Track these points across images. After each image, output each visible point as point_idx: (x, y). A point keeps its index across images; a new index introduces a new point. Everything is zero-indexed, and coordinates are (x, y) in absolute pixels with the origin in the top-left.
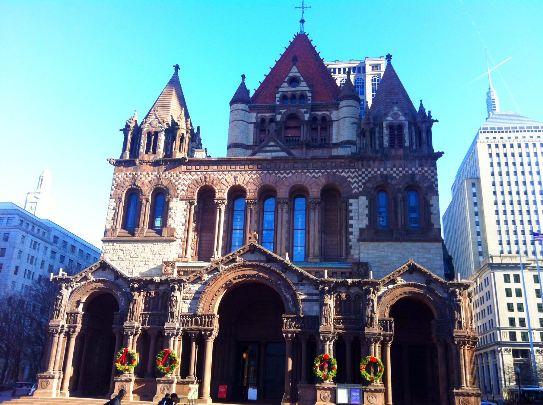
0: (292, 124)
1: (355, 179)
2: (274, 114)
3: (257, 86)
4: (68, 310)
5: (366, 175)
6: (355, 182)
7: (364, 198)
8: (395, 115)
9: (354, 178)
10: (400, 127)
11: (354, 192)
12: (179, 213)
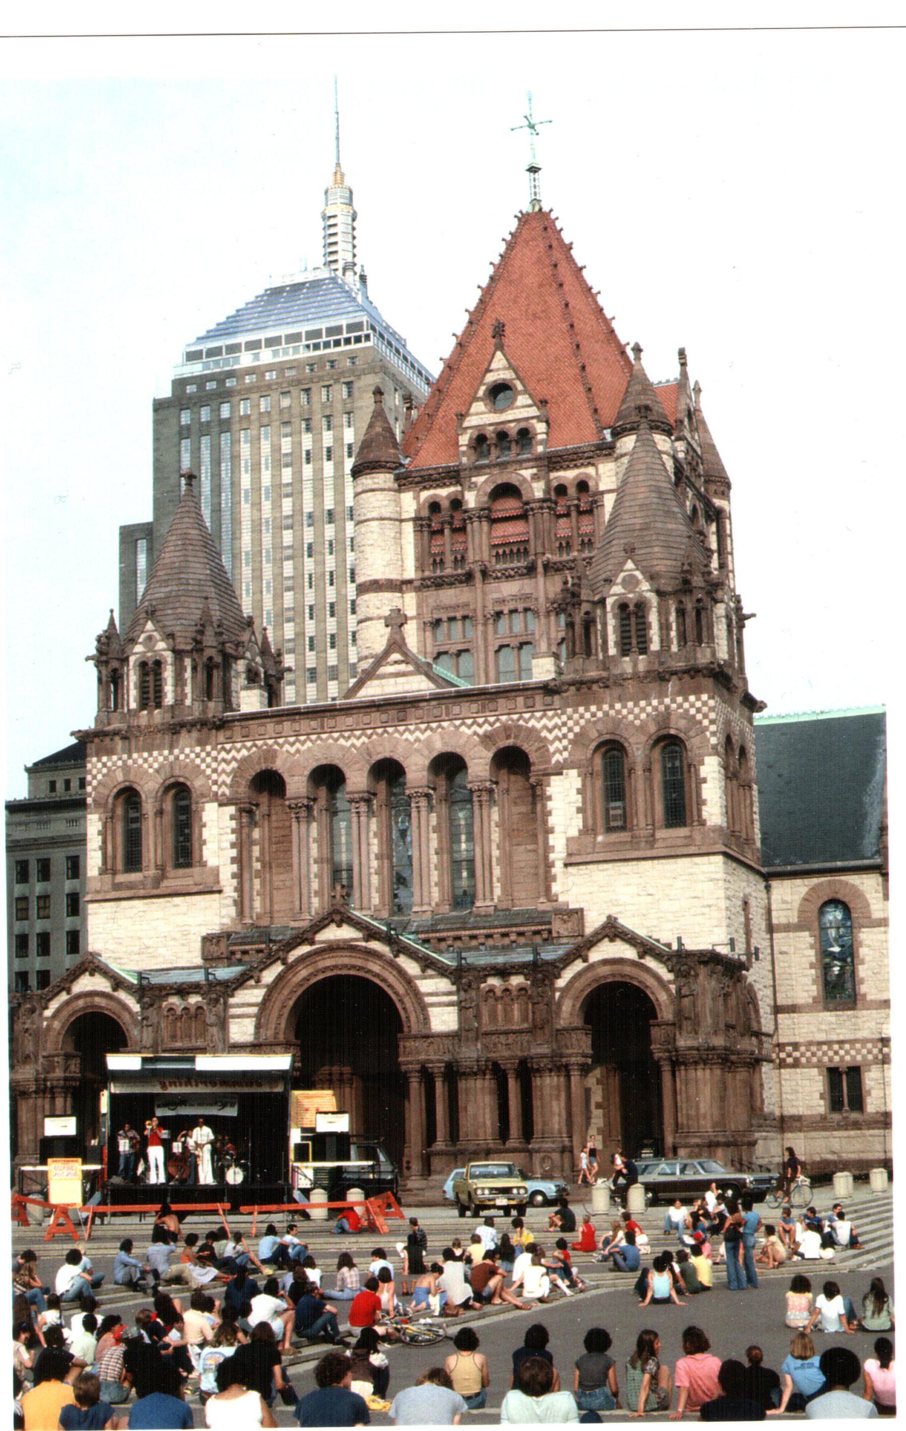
0: (509, 506)
1: (556, 732)
2: (459, 488)
3: (447, 347)
4: (228, 1227)
5: (577, 723)
6: (557, 738)
7: (574, 772)
8: (630, 582)
9: (556, 731)
10: (641, 606)
11: (554, 760)
12: (217, 828)
